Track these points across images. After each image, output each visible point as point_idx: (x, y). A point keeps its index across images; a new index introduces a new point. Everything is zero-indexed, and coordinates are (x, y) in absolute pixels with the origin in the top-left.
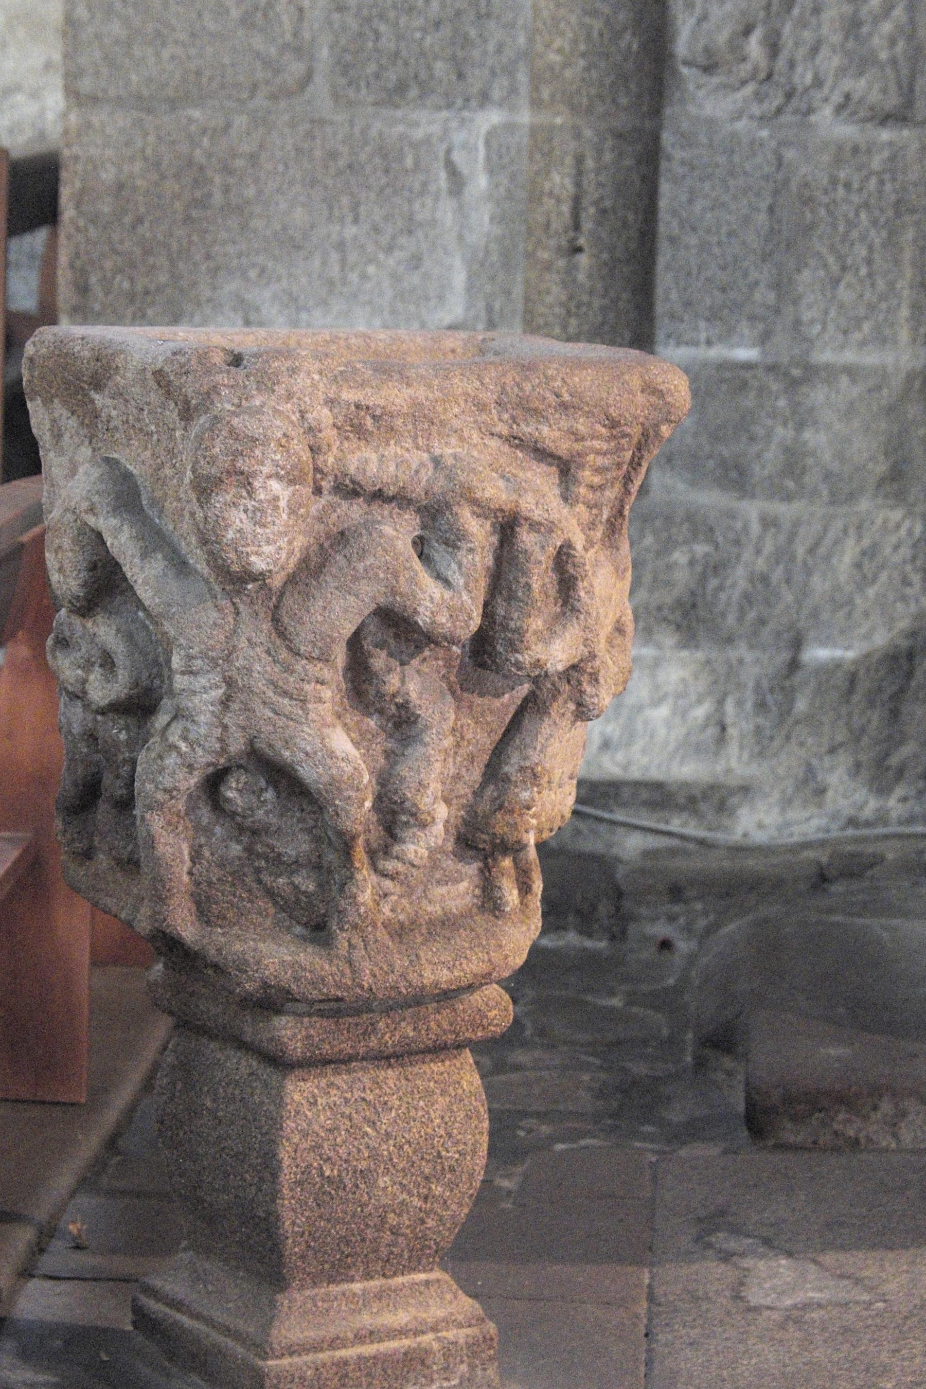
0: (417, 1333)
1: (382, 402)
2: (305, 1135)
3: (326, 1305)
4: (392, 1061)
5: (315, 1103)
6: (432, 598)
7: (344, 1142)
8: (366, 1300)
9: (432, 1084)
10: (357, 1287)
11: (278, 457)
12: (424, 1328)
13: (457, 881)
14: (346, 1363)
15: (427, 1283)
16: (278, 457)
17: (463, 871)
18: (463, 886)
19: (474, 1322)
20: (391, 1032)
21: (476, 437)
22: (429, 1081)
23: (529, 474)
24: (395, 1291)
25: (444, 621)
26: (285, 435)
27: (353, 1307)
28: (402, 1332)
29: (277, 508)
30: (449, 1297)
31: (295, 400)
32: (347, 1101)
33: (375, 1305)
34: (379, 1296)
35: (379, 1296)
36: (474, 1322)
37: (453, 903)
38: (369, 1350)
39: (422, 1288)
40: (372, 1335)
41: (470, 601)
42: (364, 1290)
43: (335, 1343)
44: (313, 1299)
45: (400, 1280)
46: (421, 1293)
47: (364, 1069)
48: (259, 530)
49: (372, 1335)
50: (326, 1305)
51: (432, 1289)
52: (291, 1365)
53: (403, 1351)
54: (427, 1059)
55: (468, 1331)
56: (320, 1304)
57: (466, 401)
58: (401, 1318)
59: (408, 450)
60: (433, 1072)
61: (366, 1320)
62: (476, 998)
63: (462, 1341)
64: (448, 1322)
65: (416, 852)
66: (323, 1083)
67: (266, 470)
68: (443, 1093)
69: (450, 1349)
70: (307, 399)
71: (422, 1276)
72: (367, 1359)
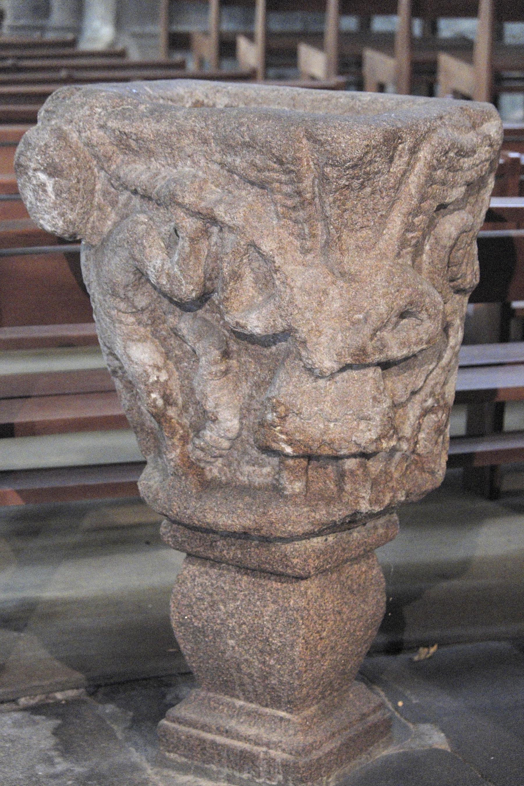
0: (257, 744)
1: (133, 130)
2: (184, 596)
3: (215, 705)
4: (249, 571)
5: (194, 580)
6: (154, 266)
7: (206, 609)
8: (240, 712)
9: (268, 594)
10: (240, 703)
11: (39, 158)
12: (260, 742)
13: (262, 466)
14: (204, 741)
15: (282, 719)
16: (39, 158)
17: (267, 460)
18: (266, 470)
19: (293, 752)
20: (255, 555)
21: (203, 162)
22: (268, 591)
23: (244, 193)
24: (259, 715)
25: (164, 283)
26: (46, 145)
27: (230, 713)
28: (246, 739)
29: (45, 191)
30: (291, 732)
31: (74, 124)
32: (212, 585)
33: (244, 717)
34: (249, 714)
35: (249, 714)
36: (293, 752)
37: (258, 479)
38: (220, 739)
39: (277, 720)
40: (227, 733)
41: (179, 273)
42: (241, 707)
43: (204, 727)
44: (210, 699)
45: (268, 710)
46: (275, 723)
47: (228, 570)
48: (38, 204)
49: (227, 733)
50: (215, 705)
51: (283, 723)
52: (174, 728)
53: (240, 749)
54: (272, 578)
55: (285, 756)
56: (212, 703)
57: (194, 135)
58: (252, 731)
59: (163, 166)
60: (272, 587)
61: (233, 724)
62: (288, 548)
63: (279, 760)
64: (277, 745)
65: (211, 437)
66: (203, 569)
67: (33, 165)
68: (275, 602)
69: (270, 762)
70: (81, 124)
71: (282, 714)
72: (217, 745)
